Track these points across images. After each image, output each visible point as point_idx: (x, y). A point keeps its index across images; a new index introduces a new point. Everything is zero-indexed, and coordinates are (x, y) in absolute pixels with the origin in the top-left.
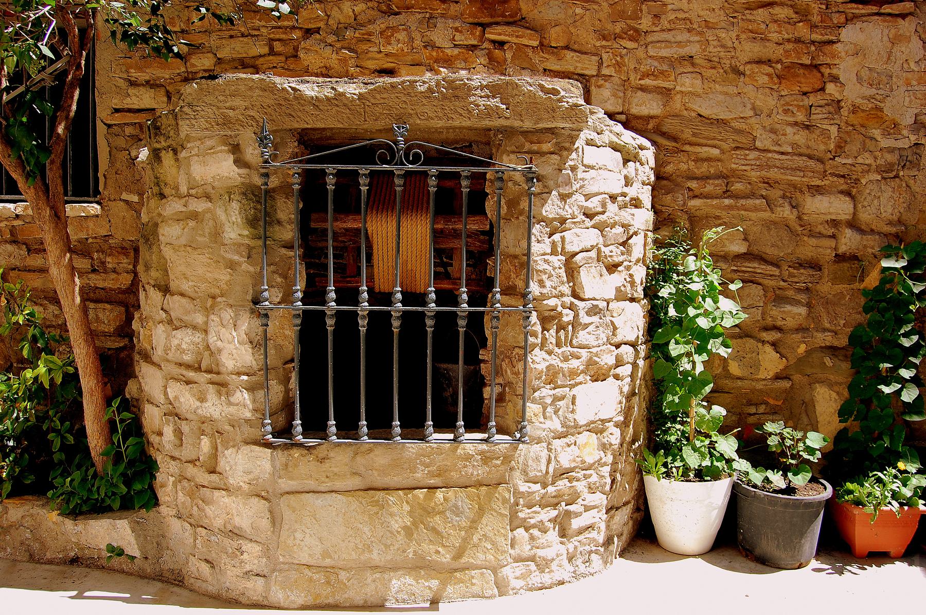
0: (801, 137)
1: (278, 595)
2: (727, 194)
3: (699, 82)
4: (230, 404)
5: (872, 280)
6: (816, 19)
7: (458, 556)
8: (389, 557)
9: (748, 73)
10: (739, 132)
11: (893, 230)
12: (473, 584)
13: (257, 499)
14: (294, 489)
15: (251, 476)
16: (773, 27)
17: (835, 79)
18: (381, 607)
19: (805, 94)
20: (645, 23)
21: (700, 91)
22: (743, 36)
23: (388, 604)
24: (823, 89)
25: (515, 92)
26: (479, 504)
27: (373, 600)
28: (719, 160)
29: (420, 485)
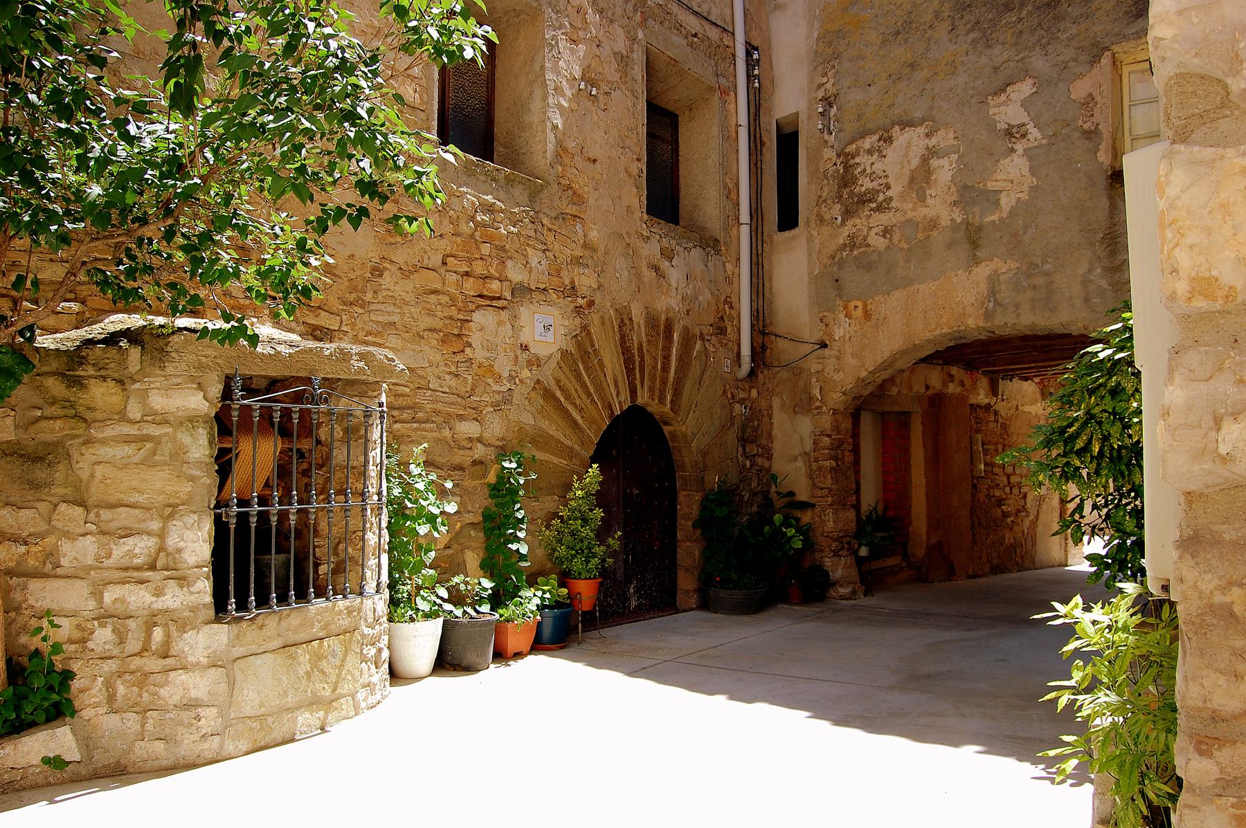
0: (453, 382)
1: (230, 747)
2: (414, 420)
3: (400, 341)
4: (191, 593)
5: (492, 478)
6: (460, 305)
7: (334, 690)
8: (297, 699)
9: (426, 337)
10: (421, 377)
11: (500, 443)
12: (342, 709)
13: (214, 669)
14: (242, 654)
15: (210, 651)
16: (439, 308)
17: (470, 345)
18: (293, 740)
19: (454, 353)
20: (369, 296)
21: (399, 347)
22: (423, 312)
23: (297, 738)
24: (463, 351)
25: (372, 359)
26: (345, 647)
27: (288, 736)
28: (408, 396)
29: (314, 638)
